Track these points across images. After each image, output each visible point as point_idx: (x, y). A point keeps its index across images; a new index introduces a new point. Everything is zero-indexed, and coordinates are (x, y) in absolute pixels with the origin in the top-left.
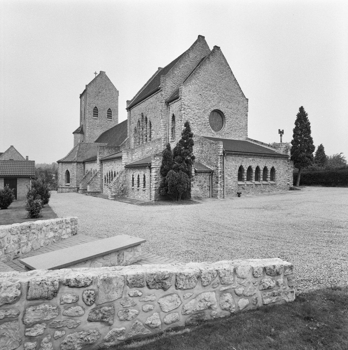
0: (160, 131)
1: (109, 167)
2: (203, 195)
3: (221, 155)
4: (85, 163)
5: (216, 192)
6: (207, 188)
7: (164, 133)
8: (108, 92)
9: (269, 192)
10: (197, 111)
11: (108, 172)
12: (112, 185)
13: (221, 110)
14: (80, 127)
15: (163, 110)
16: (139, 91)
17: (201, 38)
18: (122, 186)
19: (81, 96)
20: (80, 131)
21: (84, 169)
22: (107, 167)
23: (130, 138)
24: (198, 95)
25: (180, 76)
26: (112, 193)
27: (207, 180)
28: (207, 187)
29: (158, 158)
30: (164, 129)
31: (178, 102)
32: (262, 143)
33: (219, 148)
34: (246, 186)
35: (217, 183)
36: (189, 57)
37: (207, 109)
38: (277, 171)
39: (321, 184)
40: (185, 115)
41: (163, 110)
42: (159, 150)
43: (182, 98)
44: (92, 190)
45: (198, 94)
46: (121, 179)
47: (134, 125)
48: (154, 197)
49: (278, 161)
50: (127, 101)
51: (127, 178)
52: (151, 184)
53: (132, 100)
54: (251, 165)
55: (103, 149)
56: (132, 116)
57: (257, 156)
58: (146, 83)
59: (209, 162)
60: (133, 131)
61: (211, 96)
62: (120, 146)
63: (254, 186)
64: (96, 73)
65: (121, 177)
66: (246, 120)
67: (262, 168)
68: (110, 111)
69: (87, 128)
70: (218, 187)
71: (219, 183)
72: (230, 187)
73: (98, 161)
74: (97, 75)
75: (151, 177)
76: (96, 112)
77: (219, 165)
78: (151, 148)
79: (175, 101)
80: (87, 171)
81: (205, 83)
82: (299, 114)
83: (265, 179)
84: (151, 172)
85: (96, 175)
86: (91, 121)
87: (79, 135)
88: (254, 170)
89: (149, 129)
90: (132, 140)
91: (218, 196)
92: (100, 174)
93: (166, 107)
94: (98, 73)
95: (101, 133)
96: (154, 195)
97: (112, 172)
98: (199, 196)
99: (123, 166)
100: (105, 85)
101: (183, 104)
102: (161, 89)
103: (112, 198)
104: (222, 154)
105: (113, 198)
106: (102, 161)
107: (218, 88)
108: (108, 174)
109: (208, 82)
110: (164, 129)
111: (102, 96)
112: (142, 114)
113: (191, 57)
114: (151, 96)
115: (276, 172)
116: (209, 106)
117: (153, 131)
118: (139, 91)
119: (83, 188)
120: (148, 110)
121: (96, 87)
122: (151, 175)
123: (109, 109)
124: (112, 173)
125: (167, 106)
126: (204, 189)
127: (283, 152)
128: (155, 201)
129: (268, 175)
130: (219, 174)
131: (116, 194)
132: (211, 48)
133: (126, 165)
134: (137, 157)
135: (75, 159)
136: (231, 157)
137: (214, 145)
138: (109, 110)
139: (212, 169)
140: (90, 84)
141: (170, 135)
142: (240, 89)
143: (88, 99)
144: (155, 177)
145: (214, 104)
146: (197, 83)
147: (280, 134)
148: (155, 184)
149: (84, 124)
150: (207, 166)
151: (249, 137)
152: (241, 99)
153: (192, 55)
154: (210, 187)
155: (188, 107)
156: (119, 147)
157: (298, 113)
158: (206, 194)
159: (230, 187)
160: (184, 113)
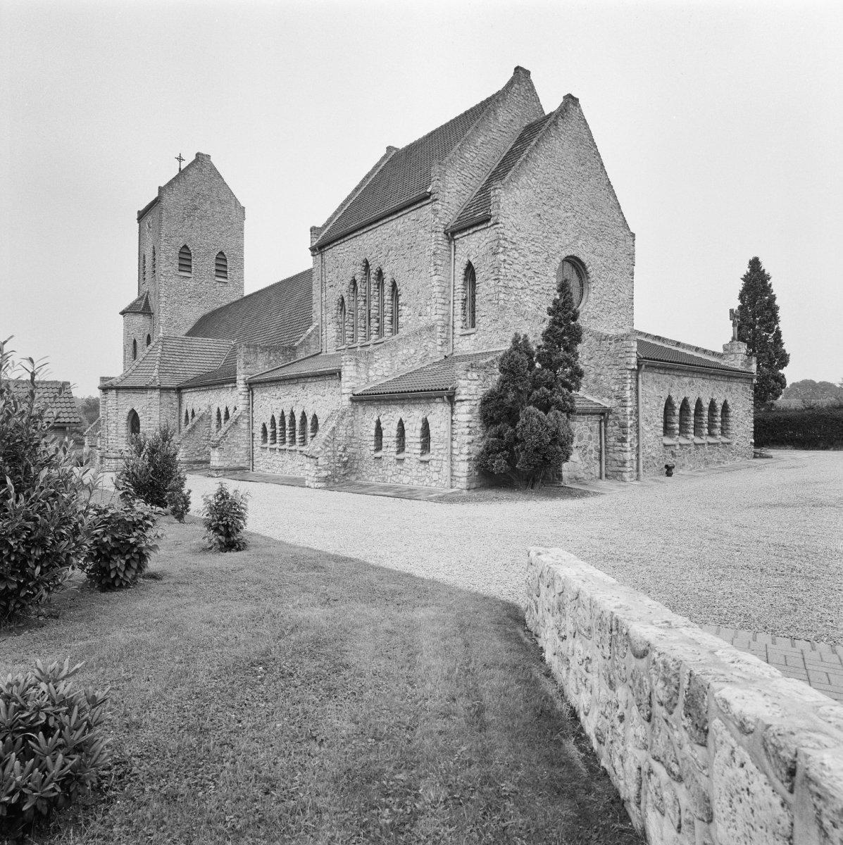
0: (428, 308)
1: (280, 401)
2: (586, 471)
3: (633, 370)
5: (620, 464)
6: (595, 454)
7: (442, 312)
8: (218, 209)
9: (719, 462)
10: (531, 257)
12: (319, 449)
13: (581, 257)
15: (439, 252)
16: (342, 204)
17: (521, 74)
18: (345, 450)
19: (142, 216)
20: (142, 308)
21: (180, 406)
22: (273, 401)
24: (534, 217)
26: (320, 470)
27: (595, 434)
28: (594, 451)
29: (475, 375)
30: (442, 301)
31: (485, 232)
32: (678, 344)
33: (628, 349)
34: (678, 447)
35: (623, 440)
36: (496, 119)
37: (553, 253)
38: (733, 412)
39: (789, 444)
40: (507, 266)
41: (439, 252)
42: (431, 355)
43: (500, 221)
44: (225, 464)
45: (534, 214)
46: (342, 431)
48: (464, 480)
49: (734, 386)
50: (313, 229)
51: (355, 429)
52: (455, 444)
53: (325, 226)
54: (687, 396)
55: (255, 352)
57: (707, 374)
58: (358, 183)
59: (594, 387)
60: (335, 306)
61: (560, 221)
62: (296, 344)
63: (693, 448)
64: (180, 159)
65: (341, 427)
66: (630, 285)
69: (164, 299)
70: (626, 451)
71: (629, 440)
72: (650, 451)
73: (241, 386)
74: (184, 165)
75: (453, 426)
76: (185, 257)
77: (628, 394)
78: (412, 351)
79: (475, 229)
80: (190, 415)
82: (749, 274)
83: (698, 432)
84: (452, 412)
85: (236, 423)
86: (173, 281)
87: (139, 320)
89: (390, 302)
90: (331, 332)
91: (626, 475)
92: (246, 421)
93: (446, 244)
94: (189, 158)
95: (200, 315)
96: (466, 474)
98: (578, 476)
99: (346, 398)
100: (210, 189)
101: (501, 236)
102: (436, 196)
103: (320, 485)
104: (636, 367)
105: (323, 485)
106: (251, 385)
107: (575, 203)
109: (555, 185)
110: (442, 301)
111: (201, 218)
112: (366, 262)
113: (500, 120)
115: (731, 414)
116: (557, 245)
117: (403, 308)
118: (343, 205)
119: (186, 457)
121: (186, 193)
122: (452, 420)
123: (221, 253)
125: (450, 243)
126: (588, 455)
127: (742, 364)
128: (469, 489)
129: (716, 422)
130: (629, 417)
131: (330, 473)
133: (354, 395)
134: (379, 373)
135: (154, 380)
136: (651, 375)
137: (610, 344)
138: (221, 257)
139: (608, 406)
140: (170, 184)
141: (459, 317)
142: (620, 207)
143: (164, 223)
144: (468, 427)
145: (567, 242)
147: (732, 322)
148: (469, 443)
149: (152, 292)
150: (589, 397)
151: (635, 328)
152: (620, 234)
153: (503, 115)
154: (601, 452)
155: (513, 247)
156: (295, 349)
157: (745, 273)
158: (592, 470)
159: (650, 451)
160: (505, 261)
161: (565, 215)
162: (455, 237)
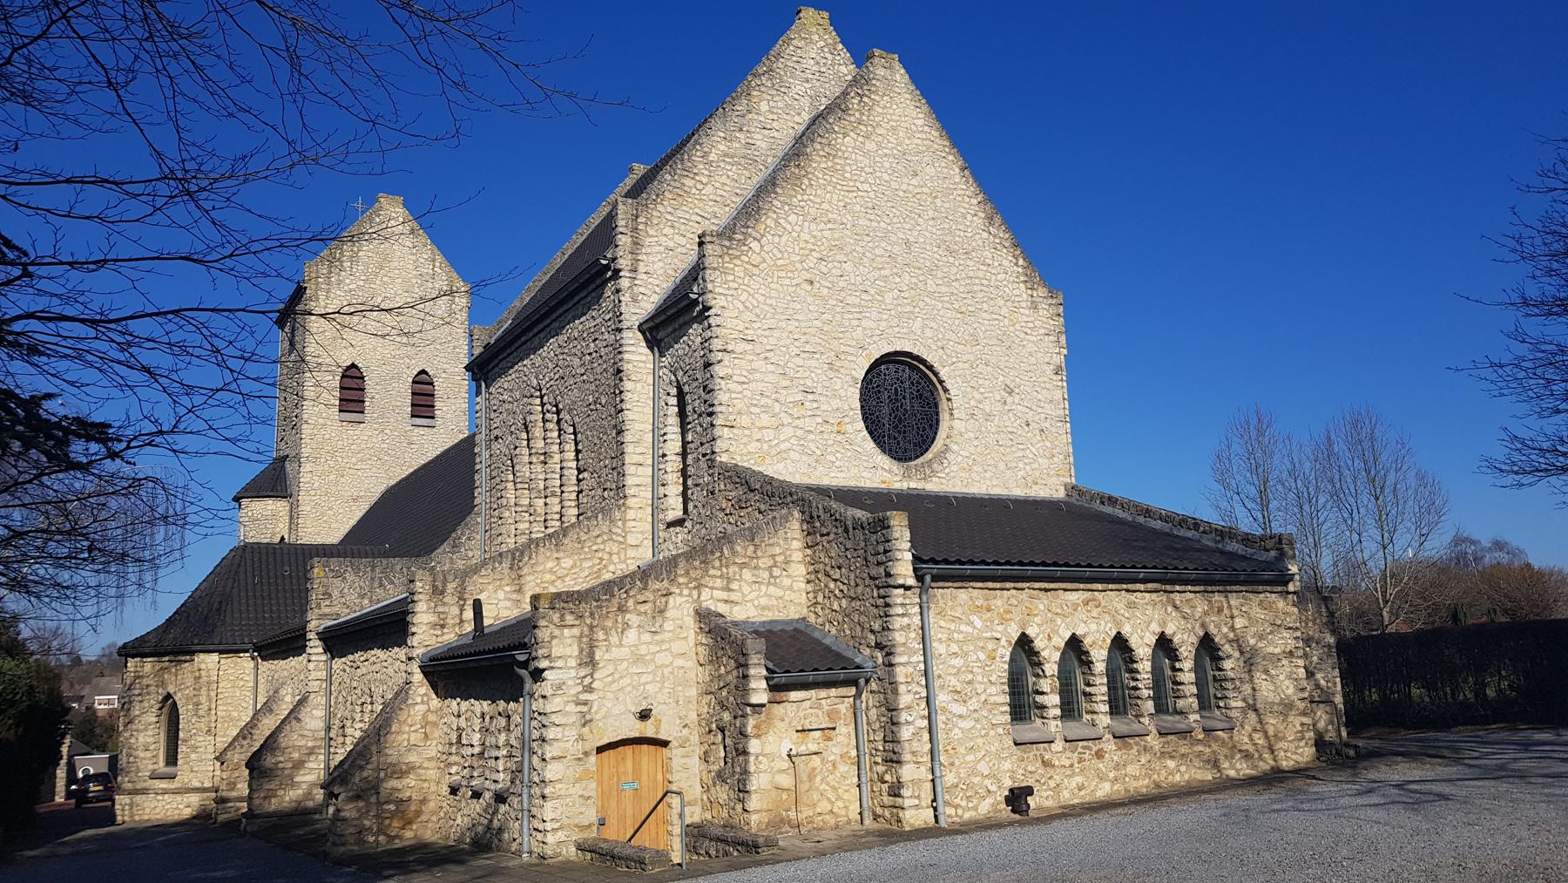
67: (1143, 647)
88: (1099, 656)
136: (963, 595)
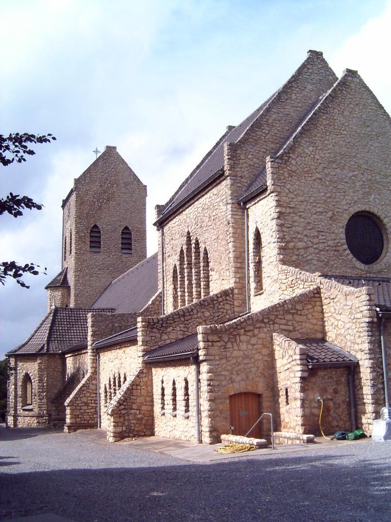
1: (113, 364)
4: (66, 356)
11: (112, 377)
14: (60, 275)
17: (315, 58)
23: (165, 292)
25: (270, 140)
47: (173, 260)
53: (167, 204)
56: (167, 240)
68: (98, 230)
74: (99, 155)
81: (328, 151)
87: (58, 294)
94: (102, 150)
97: (119, 375)
108: (112, 380)
112: (188, 233)
114: (206, 191)
120: (200, 225)
123: (126, 228)
124: (120, 378)
132: (340, 74)
145: (356, 198)
146: (309, 153)
161: (351, 174)
162: (247, 207)
